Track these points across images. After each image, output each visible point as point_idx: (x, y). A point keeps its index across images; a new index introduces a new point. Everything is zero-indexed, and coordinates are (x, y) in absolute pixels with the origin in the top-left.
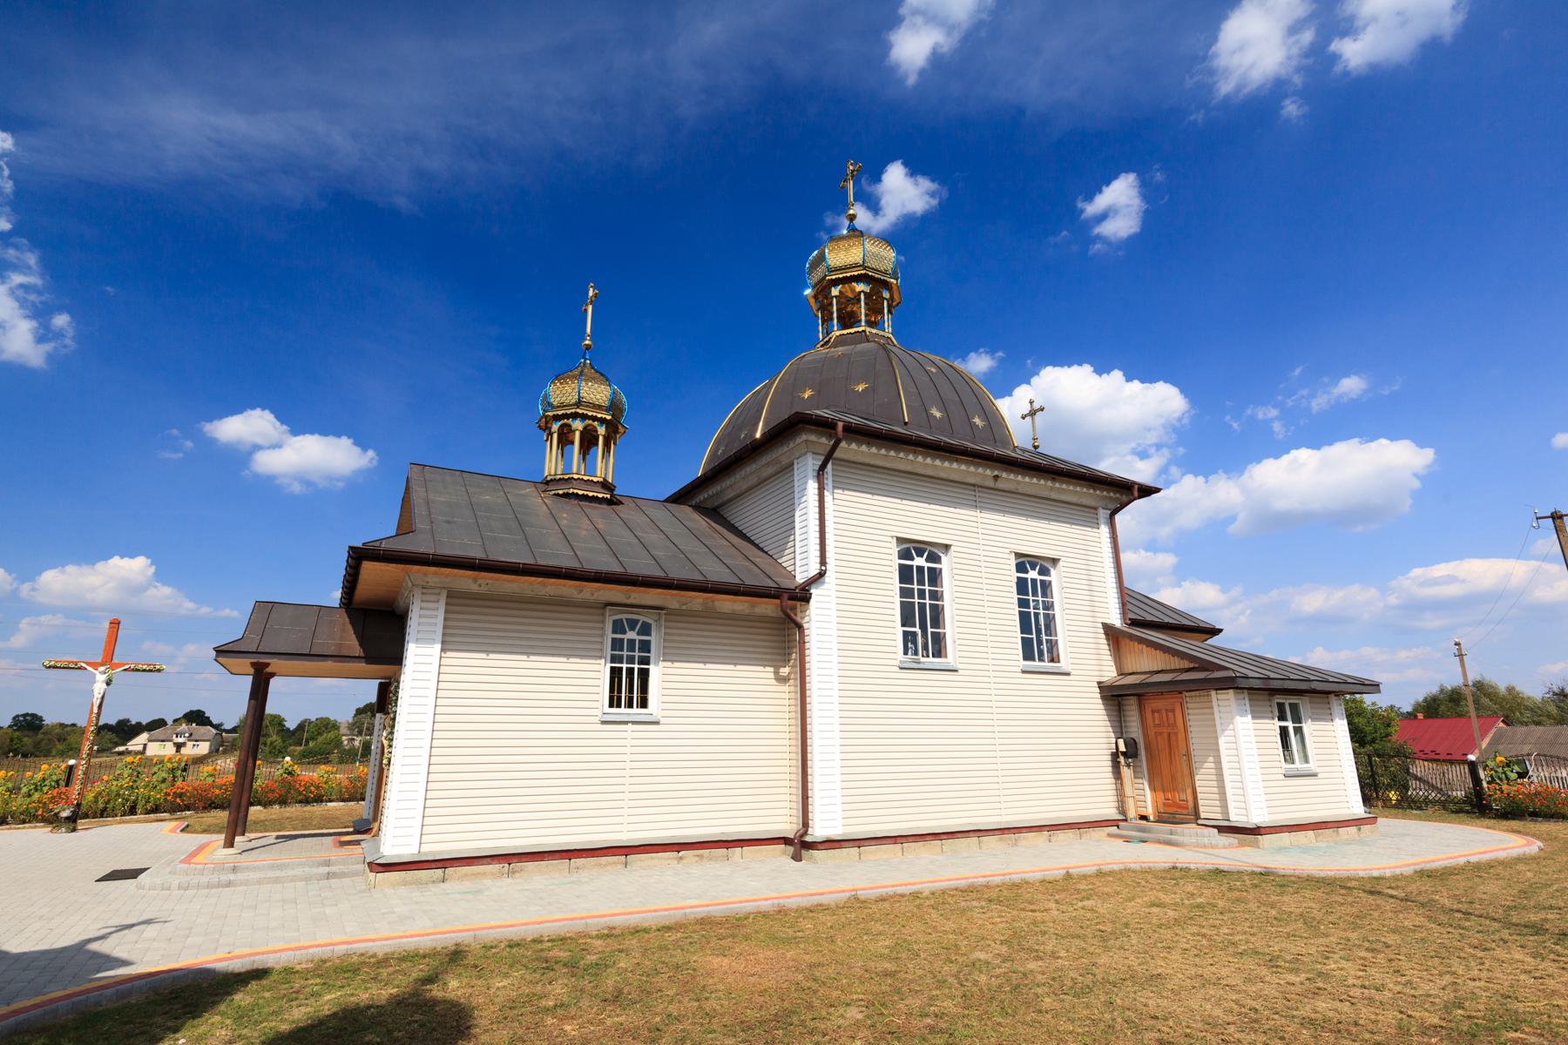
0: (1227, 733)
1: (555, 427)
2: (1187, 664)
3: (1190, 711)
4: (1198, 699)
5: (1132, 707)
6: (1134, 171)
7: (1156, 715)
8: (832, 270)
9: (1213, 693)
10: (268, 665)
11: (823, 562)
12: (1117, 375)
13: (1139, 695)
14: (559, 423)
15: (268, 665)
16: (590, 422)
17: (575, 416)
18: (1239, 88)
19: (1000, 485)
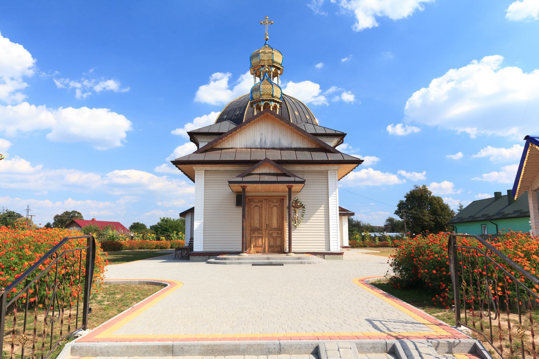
9: (343, 216)
10: (246, 186)
15: (246, 186)
17: (271, 100)
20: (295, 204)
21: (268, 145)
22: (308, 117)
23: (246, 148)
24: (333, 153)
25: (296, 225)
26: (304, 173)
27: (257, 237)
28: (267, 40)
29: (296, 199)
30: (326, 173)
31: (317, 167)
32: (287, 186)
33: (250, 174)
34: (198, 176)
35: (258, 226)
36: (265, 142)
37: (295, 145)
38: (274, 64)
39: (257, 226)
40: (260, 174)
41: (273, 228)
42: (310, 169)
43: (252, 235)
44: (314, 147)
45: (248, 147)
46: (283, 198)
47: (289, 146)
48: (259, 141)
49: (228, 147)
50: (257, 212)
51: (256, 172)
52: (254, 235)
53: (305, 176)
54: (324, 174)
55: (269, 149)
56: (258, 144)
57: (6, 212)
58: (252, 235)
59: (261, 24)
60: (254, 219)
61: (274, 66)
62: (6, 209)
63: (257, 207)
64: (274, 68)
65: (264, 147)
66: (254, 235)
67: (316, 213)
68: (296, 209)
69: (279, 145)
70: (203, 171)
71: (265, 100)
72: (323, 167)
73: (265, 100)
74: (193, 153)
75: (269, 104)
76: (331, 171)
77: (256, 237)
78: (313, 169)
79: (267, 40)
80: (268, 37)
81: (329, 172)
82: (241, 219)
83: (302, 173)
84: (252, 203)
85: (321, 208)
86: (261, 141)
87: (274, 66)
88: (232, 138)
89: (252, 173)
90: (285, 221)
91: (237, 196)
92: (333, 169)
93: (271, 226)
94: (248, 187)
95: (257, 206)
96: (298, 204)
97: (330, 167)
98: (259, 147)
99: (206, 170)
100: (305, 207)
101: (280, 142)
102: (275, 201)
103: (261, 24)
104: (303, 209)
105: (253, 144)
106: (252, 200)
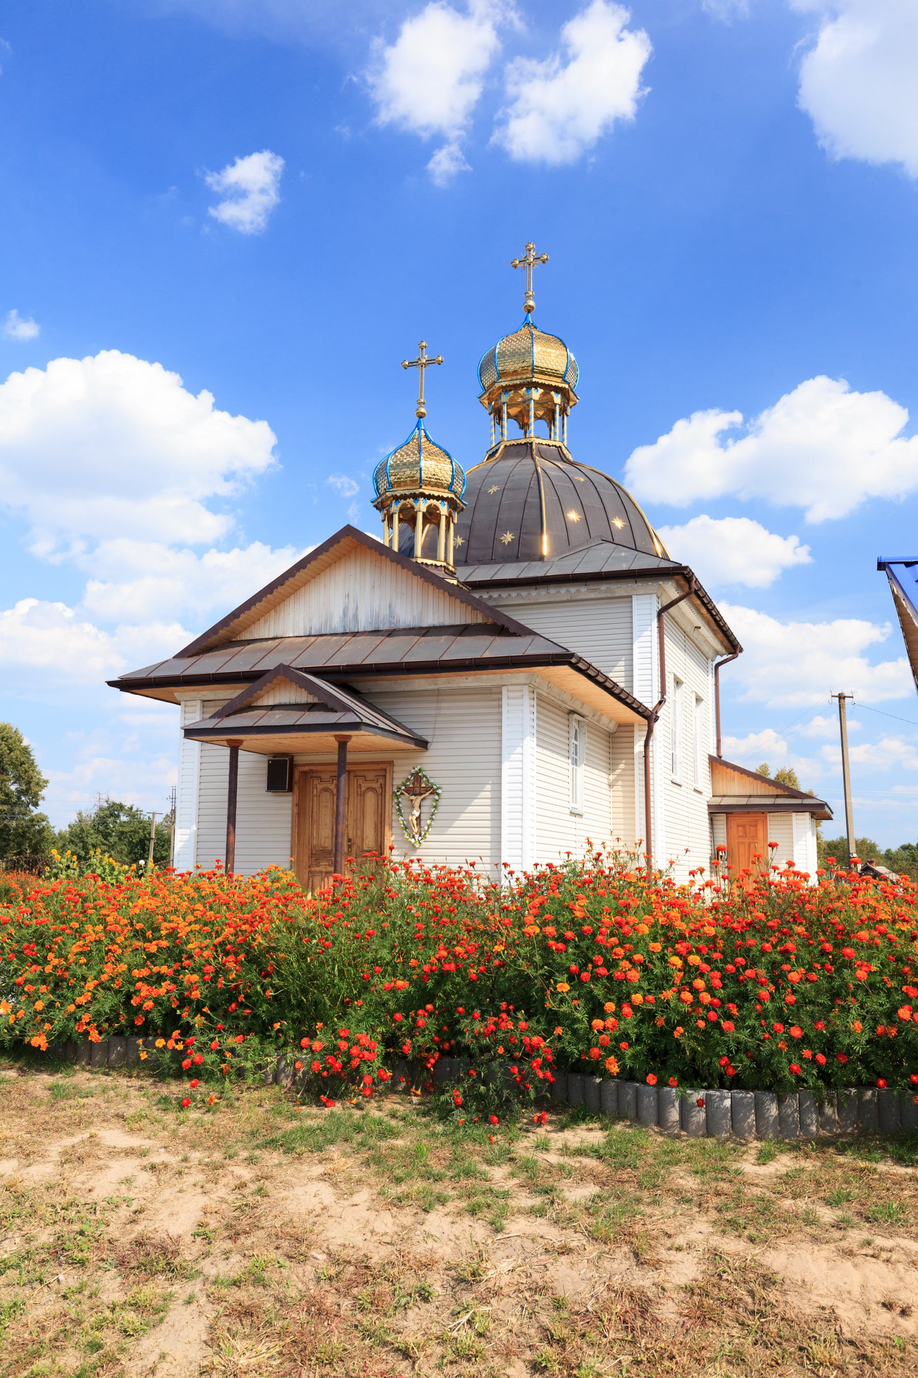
0: (800, 843)
1: (395, 508)
2: (780, 792)
3: (772, 827)
4: (779, 818)
5: (721, 819)
6: (285, 159)
7: (741, 829)
8: (502, 374)
9: (794, 814)
10: (349, 737)
11: (663, 692)
12: (207, 397)
13: (727, 813)
14: (399, 505)
15: (349, 737)
16: (403, 502)
17: (416, 497)
18: (373, 87)
19: (694, 635)
20: (413, 784)
21: (363, 624)
22: (618, 523)
23: (309, 636)
24: (514, 635)
25: (413, 840)
26: (441, 698)
27: (326, 873)
28: (529, 312)
29: (417, 769)
30: (494, 694)
31: (470, 679)
32: (336, 736)
33: (250, 708)
34: (511, 701)
35: (328, 843)
36: (356, 617)
37: (430, 620)
38: (534, 380)
39: (327, 845)
40: (272, 708)
41: (365, 848)
42: (454, 685)
43: (313, 869)
44: (480, 621)
45: (313, 633)
46: (384, 766)
47: (416, 624)
48: (341, 614)
49: (266, 637)
50: (326, 807)
51: (265, 704)
52: (317, 869)
53: (443, 705)
54: (493, 696)
55: (364, 633)
56: (337, 625)
57: (106, 805)
58: (313, 869)
59: (515, 267)
60: (318, 825)
61: (537, 385)
62: (105, 797)
63: (328, 794)
64: (541, 391)
65: (352, 630)
66: (317, 869)
67: (470, 808)
68: (413, 797)
69: (390, 623)
70: (199, 704)
71: (430, 497)
72: (485, 677)
73: (430, 497)
74: (174, 657)
75: (412, 508)
76: (510, 688)
77: (322, 872)
78: (462, 685)
79: (529, 310)
80: (531, 303)
81: (504, 689)
82: (226, 826)
83: (435, 698)
84: (316, 782)
85: (483, 794)
86: (345, 614)
87: (537, 385)
88: (276, 611)
89: (255, 704)
90: (387, 829)
91: (269, 764)
92: (514, 681)
93: (359, 844)
94: (353, 739)
95: (326, 790)
96: (423, 785)
97: (504, 676)
98: (341, 630)
99: (205, 698)
100: (439, 791)
101: (391, 615)
102: (371, 776)
103: (515, 267)
104: (432, 796)
105: (326, 622)
106: (314, 775)
